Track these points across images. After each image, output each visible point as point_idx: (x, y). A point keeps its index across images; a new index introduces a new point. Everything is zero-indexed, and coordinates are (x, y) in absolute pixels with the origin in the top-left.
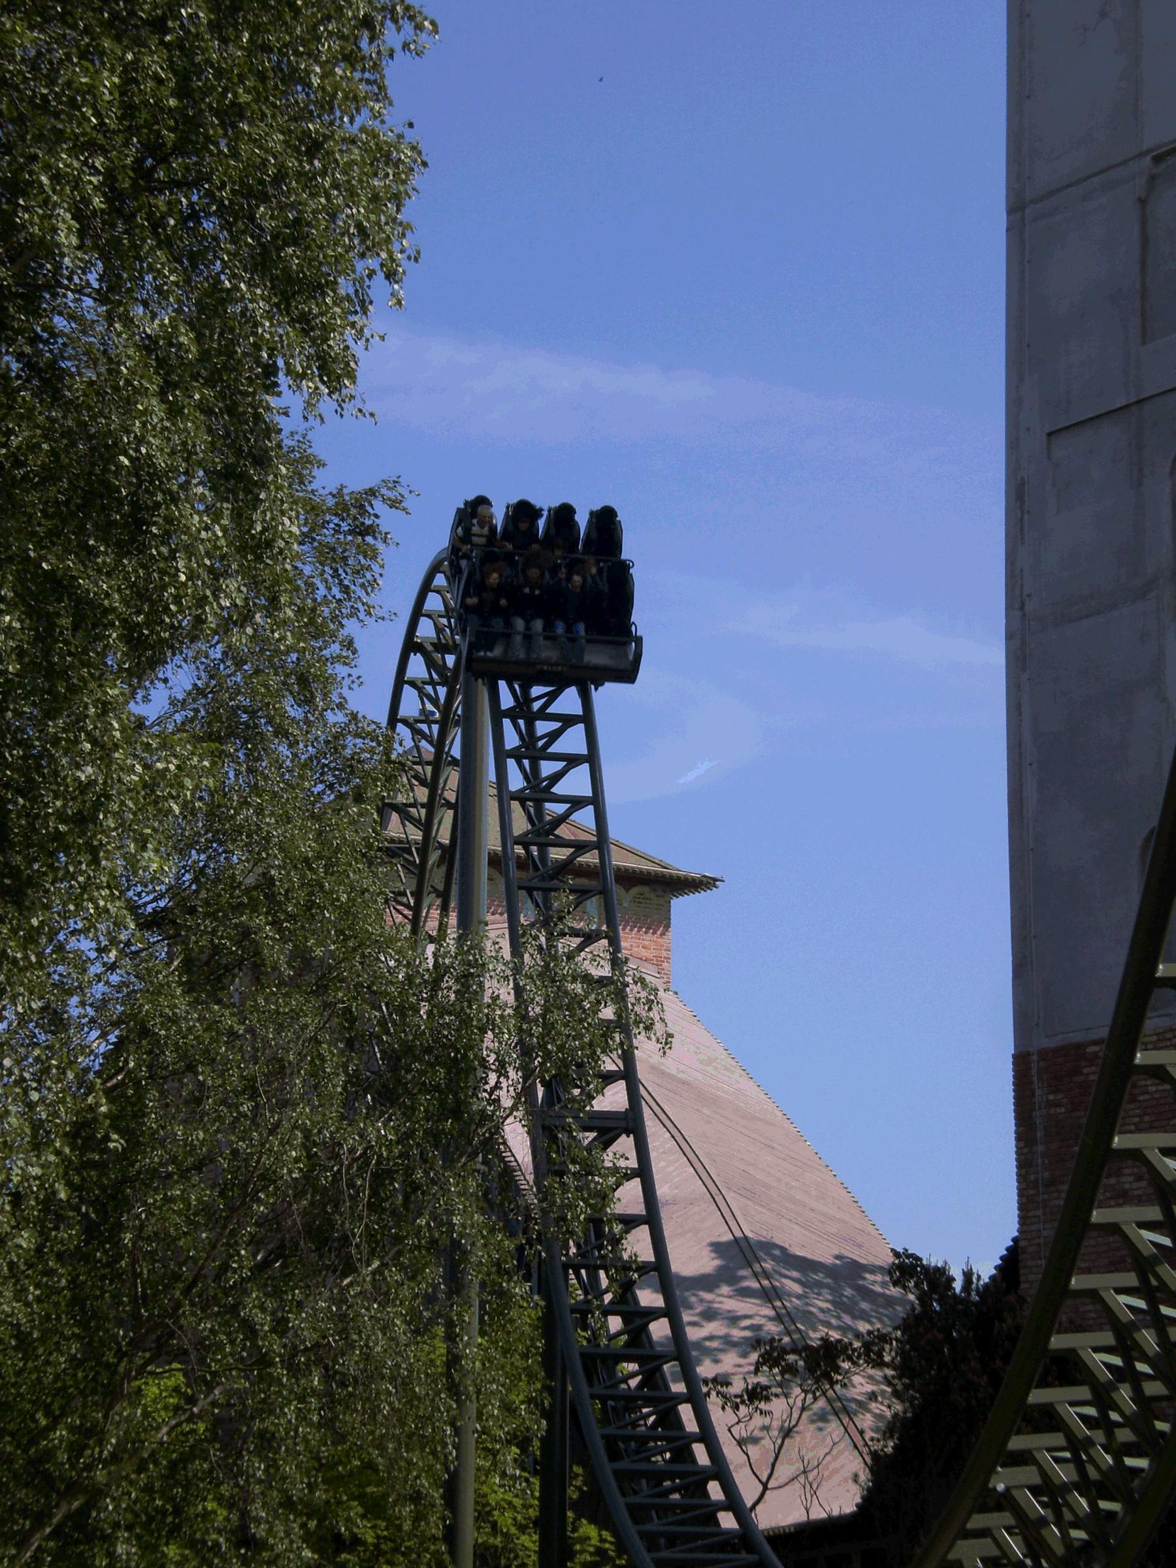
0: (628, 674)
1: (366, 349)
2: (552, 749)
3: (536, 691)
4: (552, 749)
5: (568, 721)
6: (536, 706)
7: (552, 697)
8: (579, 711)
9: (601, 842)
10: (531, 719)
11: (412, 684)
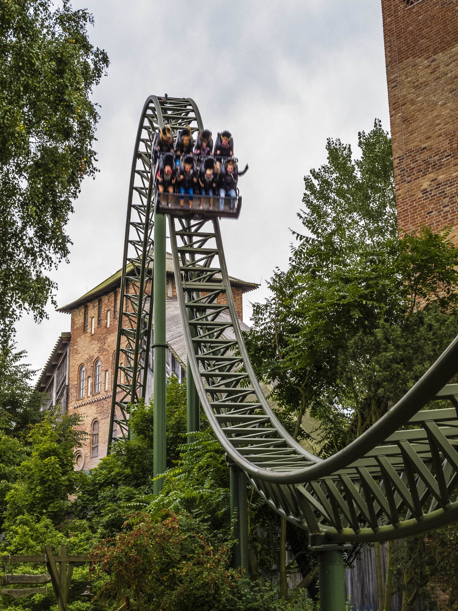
0: (235, 215)
1: (72, 244)
2: (200, 231)
3: (193, 222)
4: (200, 231)
5: (207, 236)
6: (193, 229)
7: (201, 225)
8: (213, 231)
9: (223, 269)
10: (190, 236)
11: (143, 141)
